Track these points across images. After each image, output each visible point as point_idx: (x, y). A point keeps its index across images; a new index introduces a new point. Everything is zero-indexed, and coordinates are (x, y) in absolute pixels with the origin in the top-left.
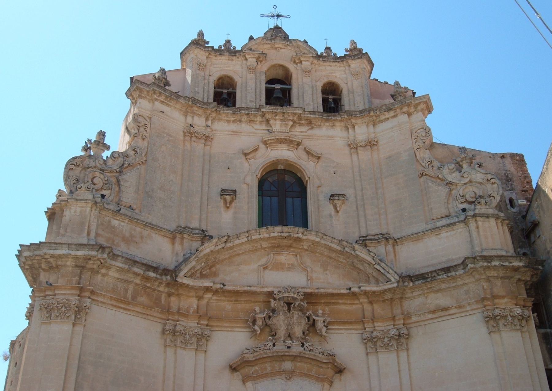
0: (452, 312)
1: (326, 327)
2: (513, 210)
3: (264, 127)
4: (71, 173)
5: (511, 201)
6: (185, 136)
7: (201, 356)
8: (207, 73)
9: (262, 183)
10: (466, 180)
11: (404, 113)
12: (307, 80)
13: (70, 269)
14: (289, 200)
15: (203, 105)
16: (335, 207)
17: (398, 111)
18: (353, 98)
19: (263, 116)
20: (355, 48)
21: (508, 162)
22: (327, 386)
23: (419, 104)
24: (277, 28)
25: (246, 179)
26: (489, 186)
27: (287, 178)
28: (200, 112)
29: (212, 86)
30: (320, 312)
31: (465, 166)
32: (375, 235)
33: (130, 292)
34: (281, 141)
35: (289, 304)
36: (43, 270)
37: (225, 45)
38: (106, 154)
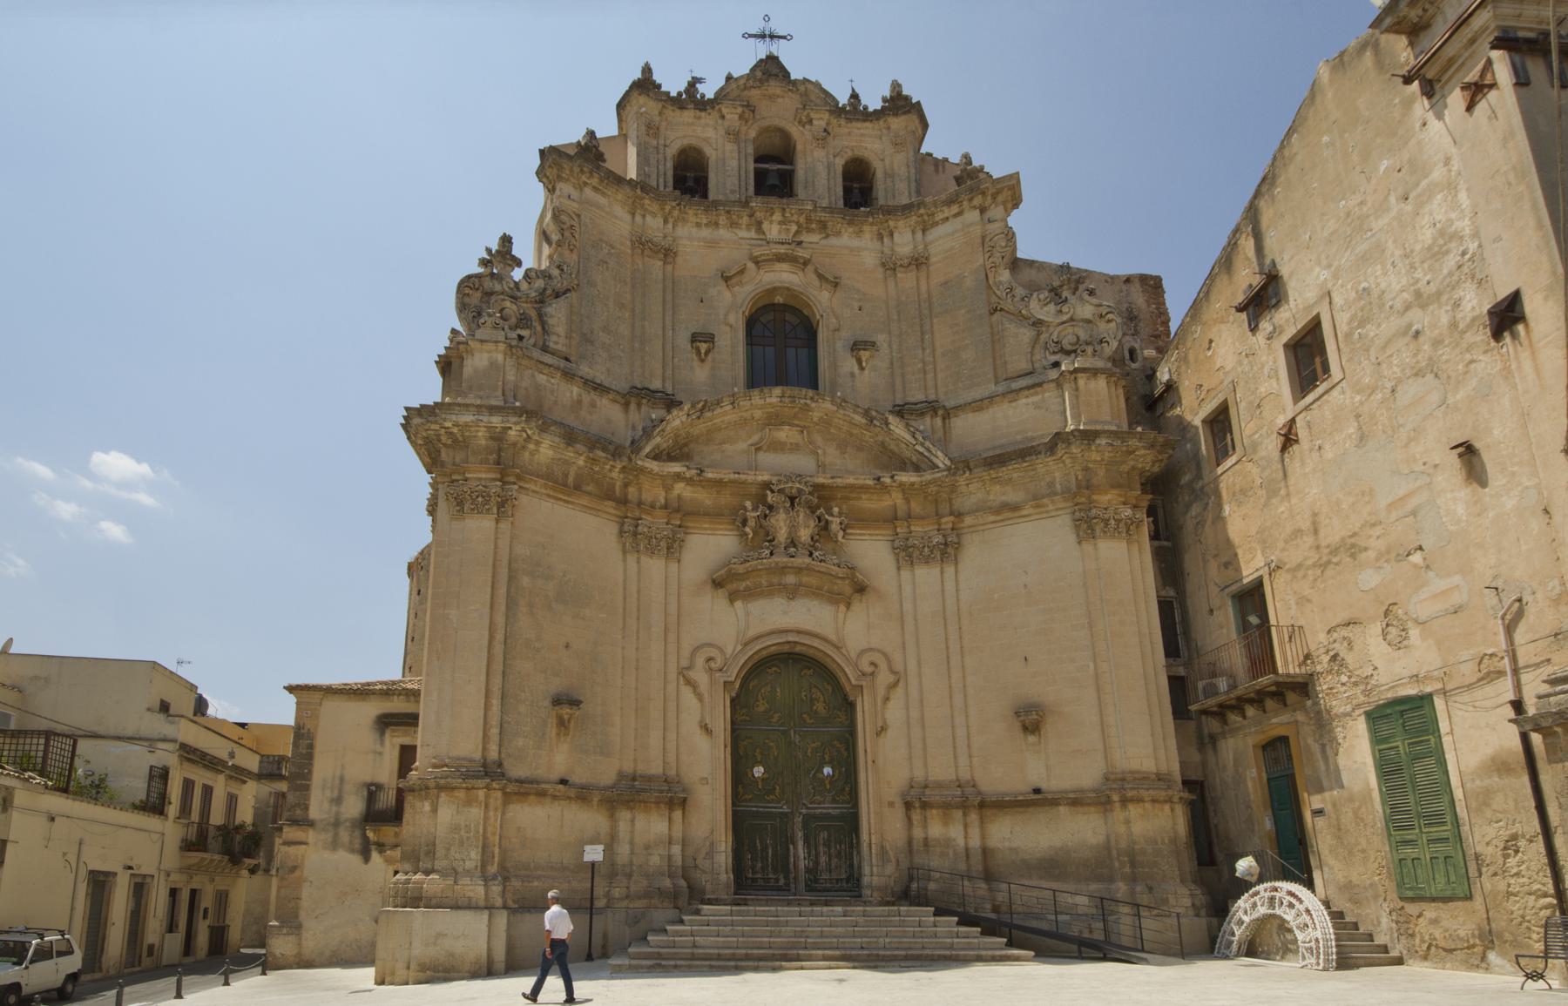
0: (1025, 512)
3: (753, 234)
4: (467, 300)
5: (1132, 352)
6: (633, 248)
7: (674, 567)
8: (661, 142)
9: (751, 323)
10: (1065, 318)
12: (819, 154)
13: (483, 442)
14: (791, 352)
15: (659, 197)
16: (859, 361)
17: (965, 203)
18: (892, 183)
19: (751, 216)
20: (899, 94)
21: (1136, 289)
22: (842, 608)
23: (999, 192)
24: (772, 60)
25: (728, 315)
26: (1102, 326)
27: (788, 317)
28: (655, 207)
29: (670, 165)
30: (836, 510)
31: (1065, 294)
34: (780, 258)
35: (792, 499)
37: (687, 91)
38: (518, 274)
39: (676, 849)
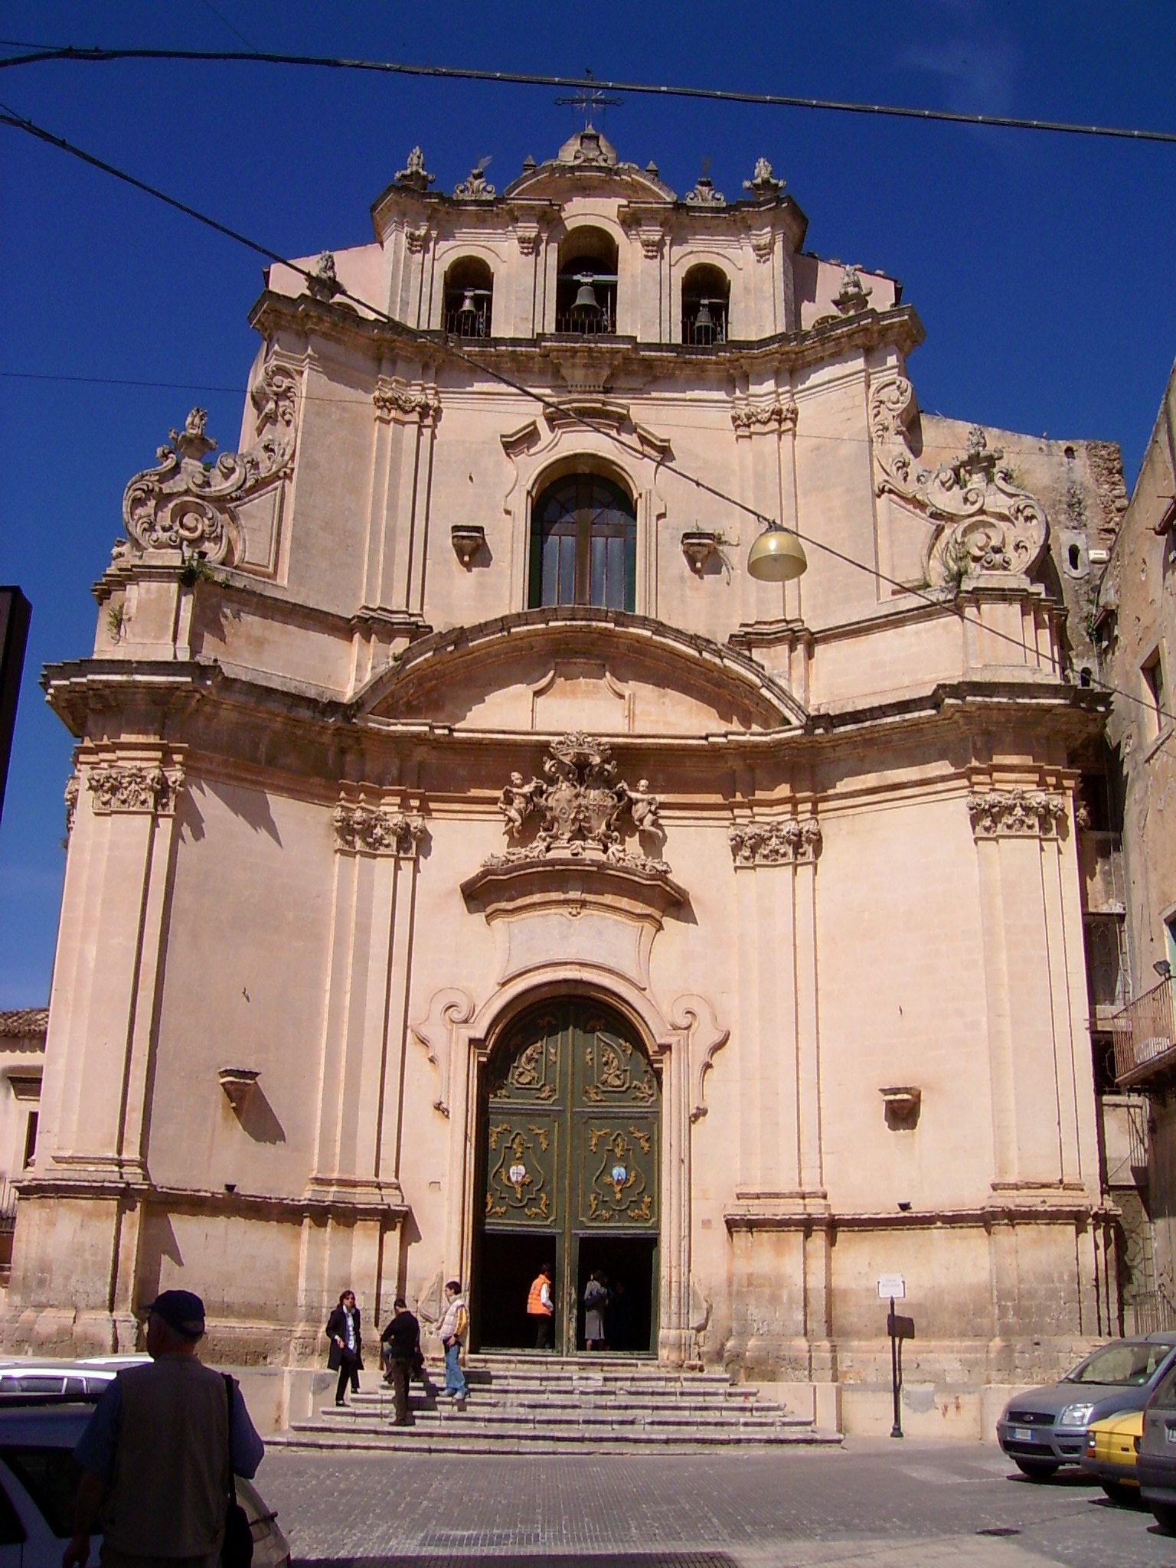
1: (654, 813)
2: (1075, 573)
11: (857, 347)
14: (599, 541)
32: (771, 623)
33: (263, 748)
36: (92, 710)
39: (87, 1256)
